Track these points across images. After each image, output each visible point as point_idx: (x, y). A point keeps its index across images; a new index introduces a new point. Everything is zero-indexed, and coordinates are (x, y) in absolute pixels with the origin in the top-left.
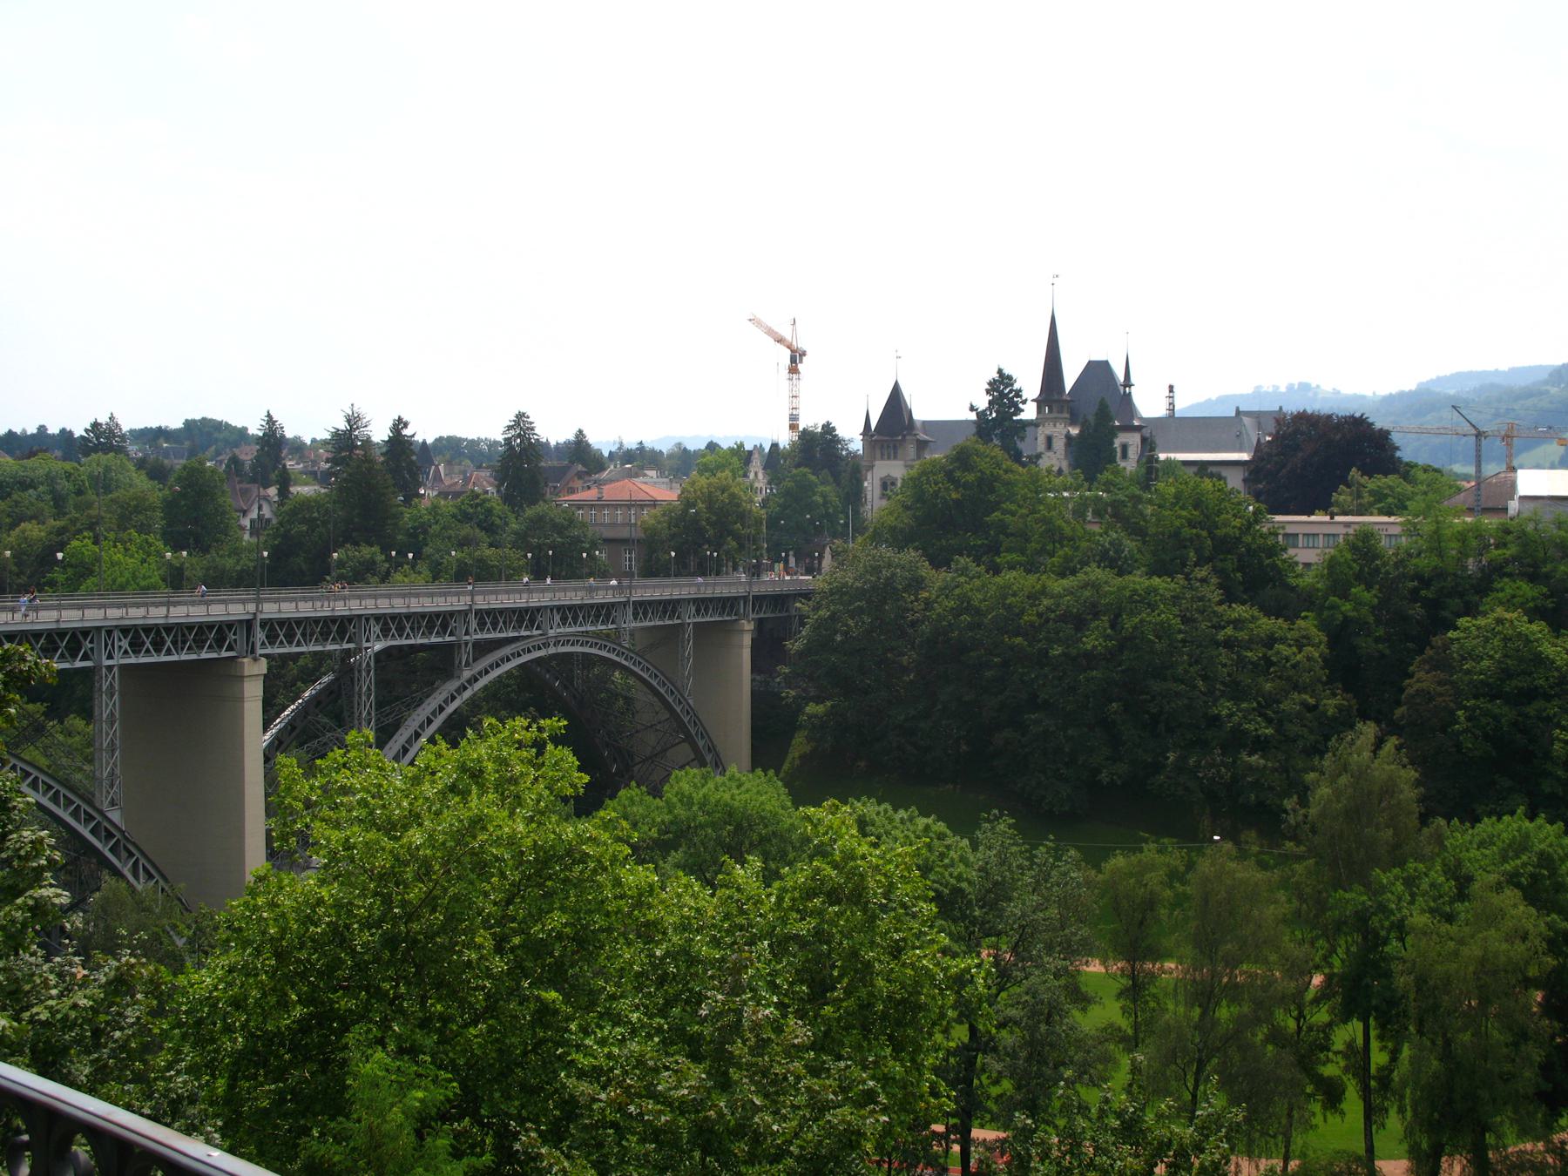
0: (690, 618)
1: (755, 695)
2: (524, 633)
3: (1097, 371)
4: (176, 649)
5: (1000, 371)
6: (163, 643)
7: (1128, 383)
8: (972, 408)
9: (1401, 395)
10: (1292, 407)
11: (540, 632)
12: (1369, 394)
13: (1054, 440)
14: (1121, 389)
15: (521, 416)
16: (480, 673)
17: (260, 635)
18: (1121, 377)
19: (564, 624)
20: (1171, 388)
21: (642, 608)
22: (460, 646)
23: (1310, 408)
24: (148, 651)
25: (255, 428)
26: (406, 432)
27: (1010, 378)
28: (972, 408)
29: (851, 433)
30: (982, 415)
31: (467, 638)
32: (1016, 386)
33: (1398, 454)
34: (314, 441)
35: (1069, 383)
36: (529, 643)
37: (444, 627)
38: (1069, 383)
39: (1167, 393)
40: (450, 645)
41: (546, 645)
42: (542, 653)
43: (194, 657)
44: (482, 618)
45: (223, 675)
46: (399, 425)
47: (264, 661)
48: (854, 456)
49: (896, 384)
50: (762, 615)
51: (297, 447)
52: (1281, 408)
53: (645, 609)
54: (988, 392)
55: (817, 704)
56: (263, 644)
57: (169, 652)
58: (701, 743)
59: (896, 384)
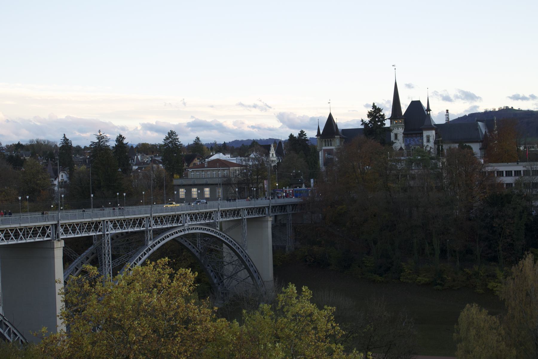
0: (245, 216)
1: (273, 247)
2: (174, 225)
3: (416, 105)
4: (25, 238)
6: (123, 225)
7: (429, 110)
11: (181, 224)
13: (398, 135)
14: (426, 112)
16: (156, 243)
19: (248, 215)
21: (224, 213)
22: (147, 232)
24: (12, 239)
26: (125, 141)
31: (150, 228)
35: (404, 110)
36: (177, 230)
37: (140, 224)
38: (404, 110)
40: (143, 232)
41: (184, 230)
42: (183, 233)
43: (32, 241)
44: (222, 213)
45: (48, 247)
47: (63, 242)
50: (276, 214)
52: (225, 142)
53: (252, 211)
56: (247, 215)
57: (21, 239)
58: (251, 269)
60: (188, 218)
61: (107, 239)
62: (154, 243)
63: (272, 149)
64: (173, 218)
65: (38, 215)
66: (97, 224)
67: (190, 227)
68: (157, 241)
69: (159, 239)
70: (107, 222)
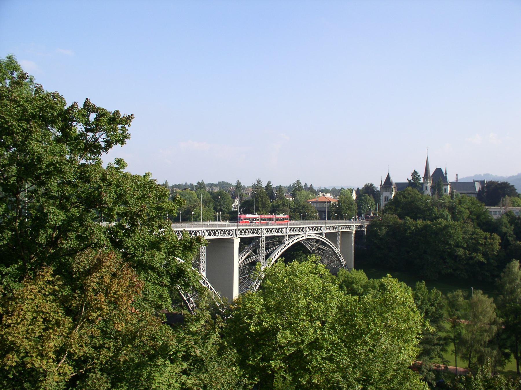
3: (439, 171)
5: (414, 171)
7: (446, 174)
8: (408, 179)
9: (513, 177)
10: (487, 180)
12: (505, 176)
15: (298, 181)
17: (238, 232)
18: (444, 172)
20: (457, 175)
23: (493, 180)
25: (234, 184)
27: (417, 172)
28: (408, 179)
29: (377, 186)
30: (410, 181)
32: (418, 174)
33: (516, 191)
34: (248, 186)
36: (301, 236)
39: (456, 176)
46: (269, 182)
47: (239, 239)
48: (378, 191)
49: (388, 174)
51: (244, 188)
54: (412, 175)
55: (500, 244)
59: (388, 174)
60: (308, 229)
61: (263, 239)
62: (289, 242)
63: (354, 192)
64: (253, 231)
65: (228, 223)
66: (258, 230)
67: (309, 235)
68: (290, 241)
69: (291, 241)
70: (204, 231)
